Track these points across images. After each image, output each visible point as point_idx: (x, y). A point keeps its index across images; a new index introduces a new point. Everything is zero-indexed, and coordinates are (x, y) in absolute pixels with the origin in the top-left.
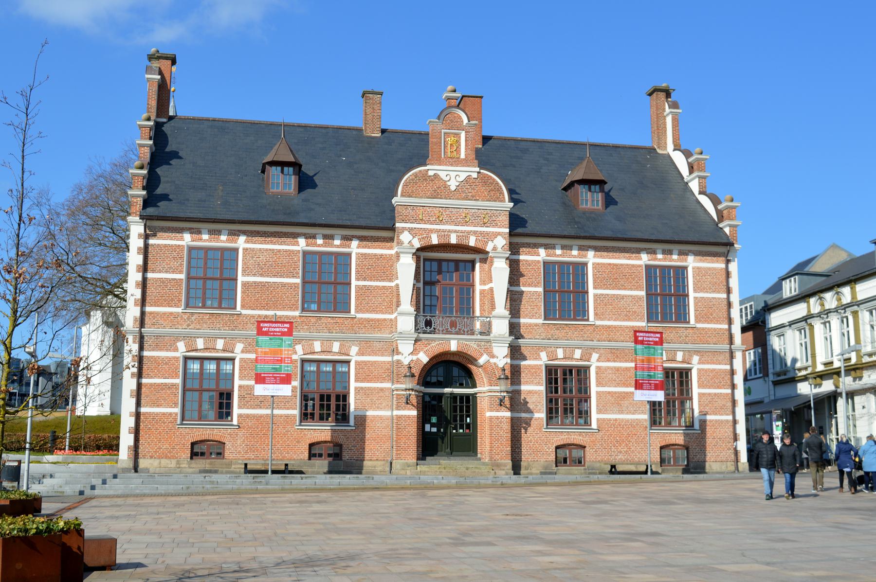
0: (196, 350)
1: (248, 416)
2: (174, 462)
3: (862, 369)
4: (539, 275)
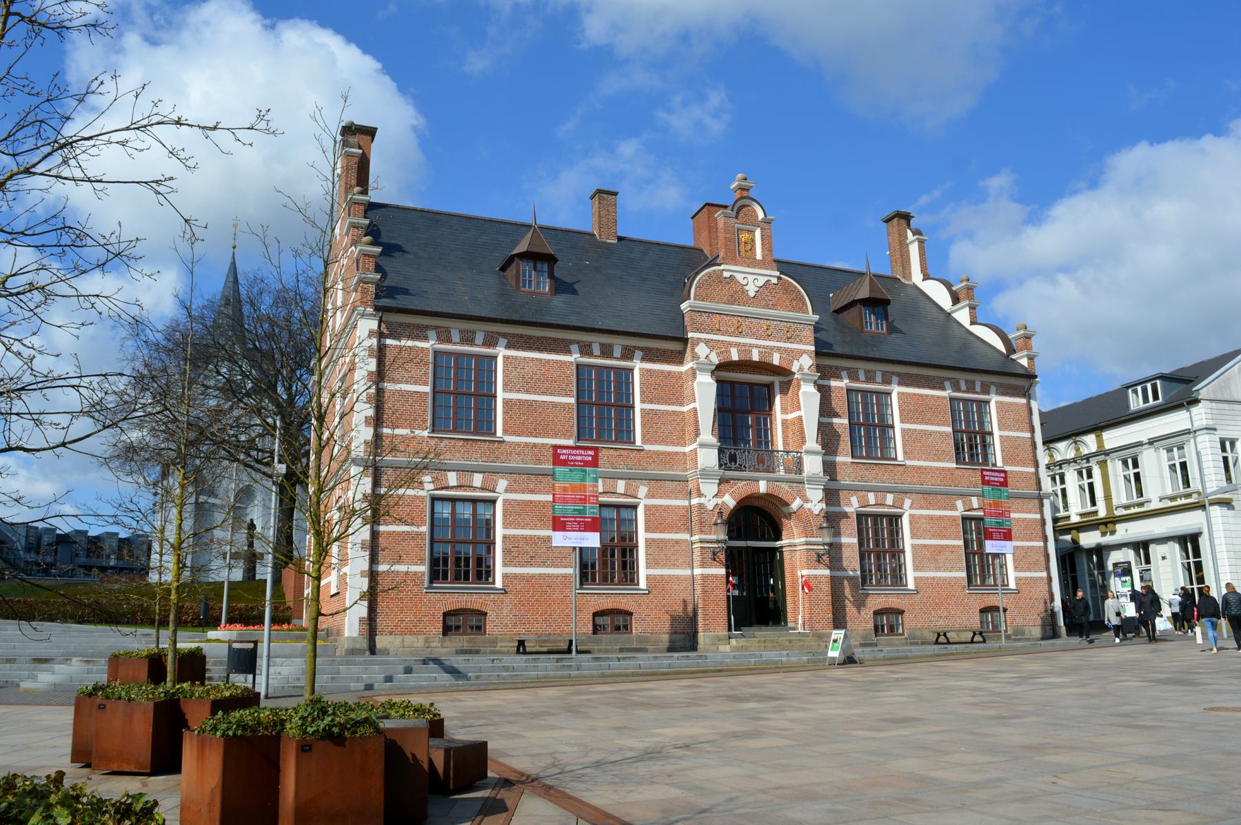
0: (447, 488)
1: (515, 576)
2: (421, 638)
3: (1114, 523)
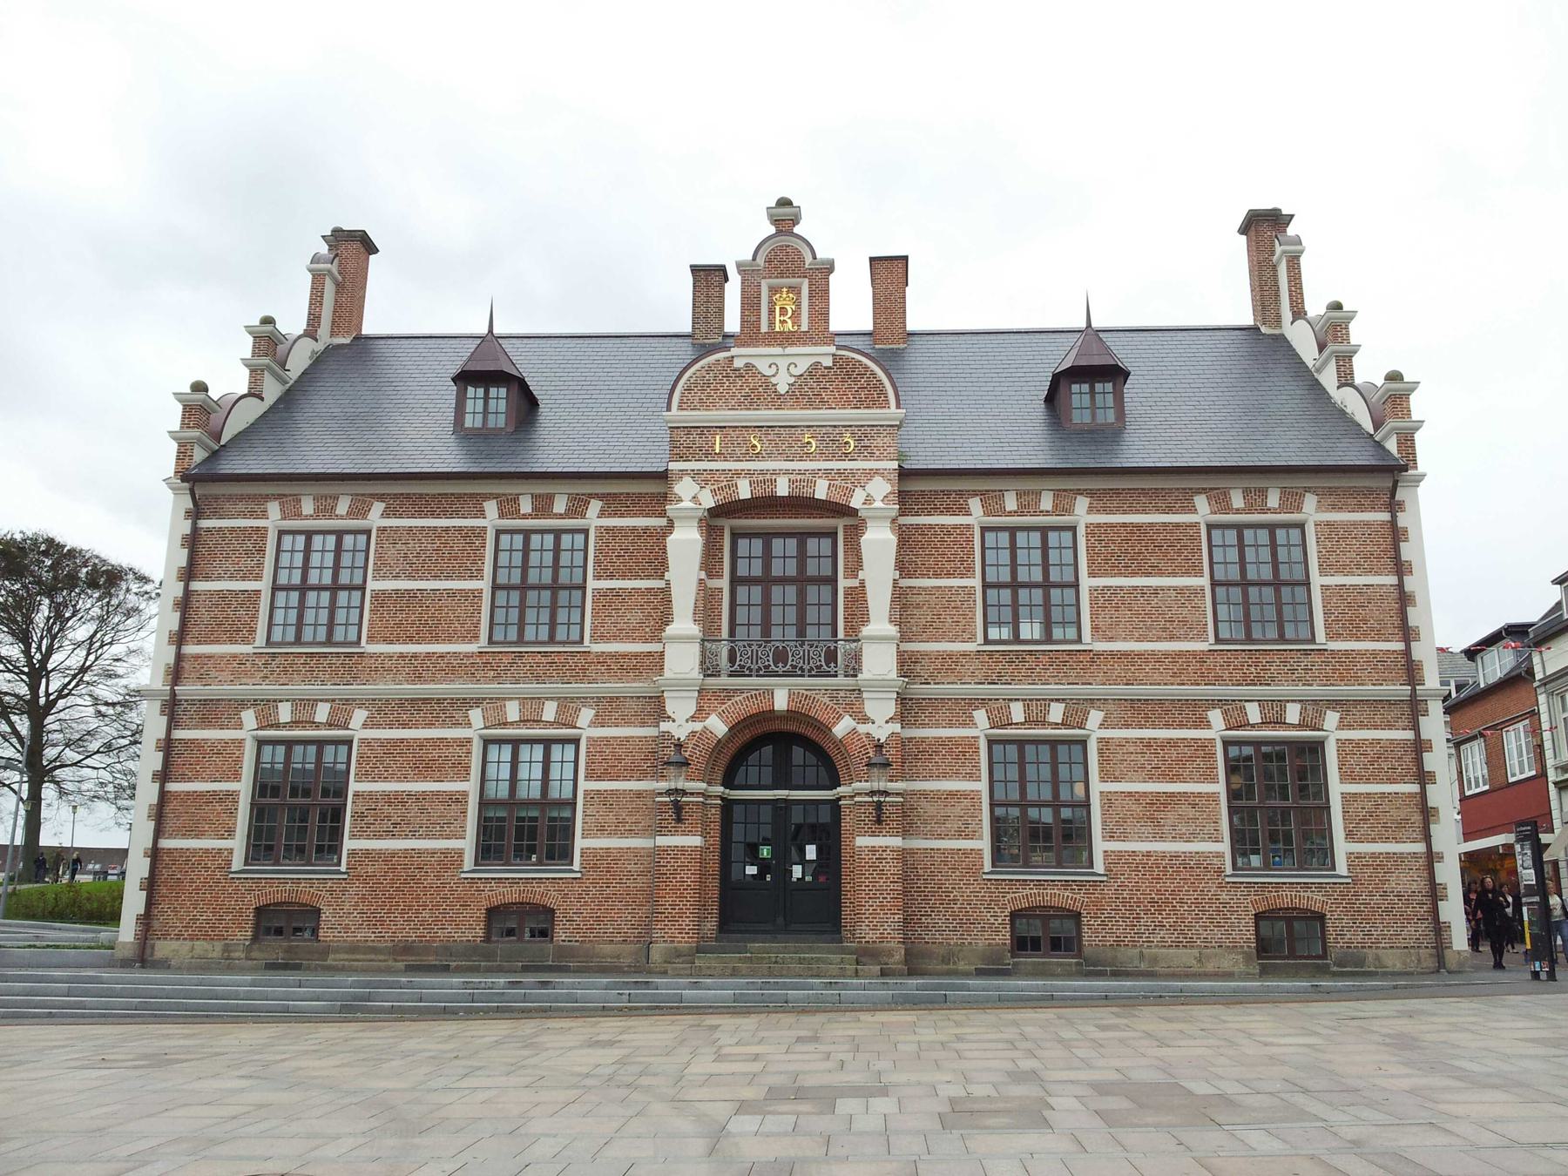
1: (367, 853)
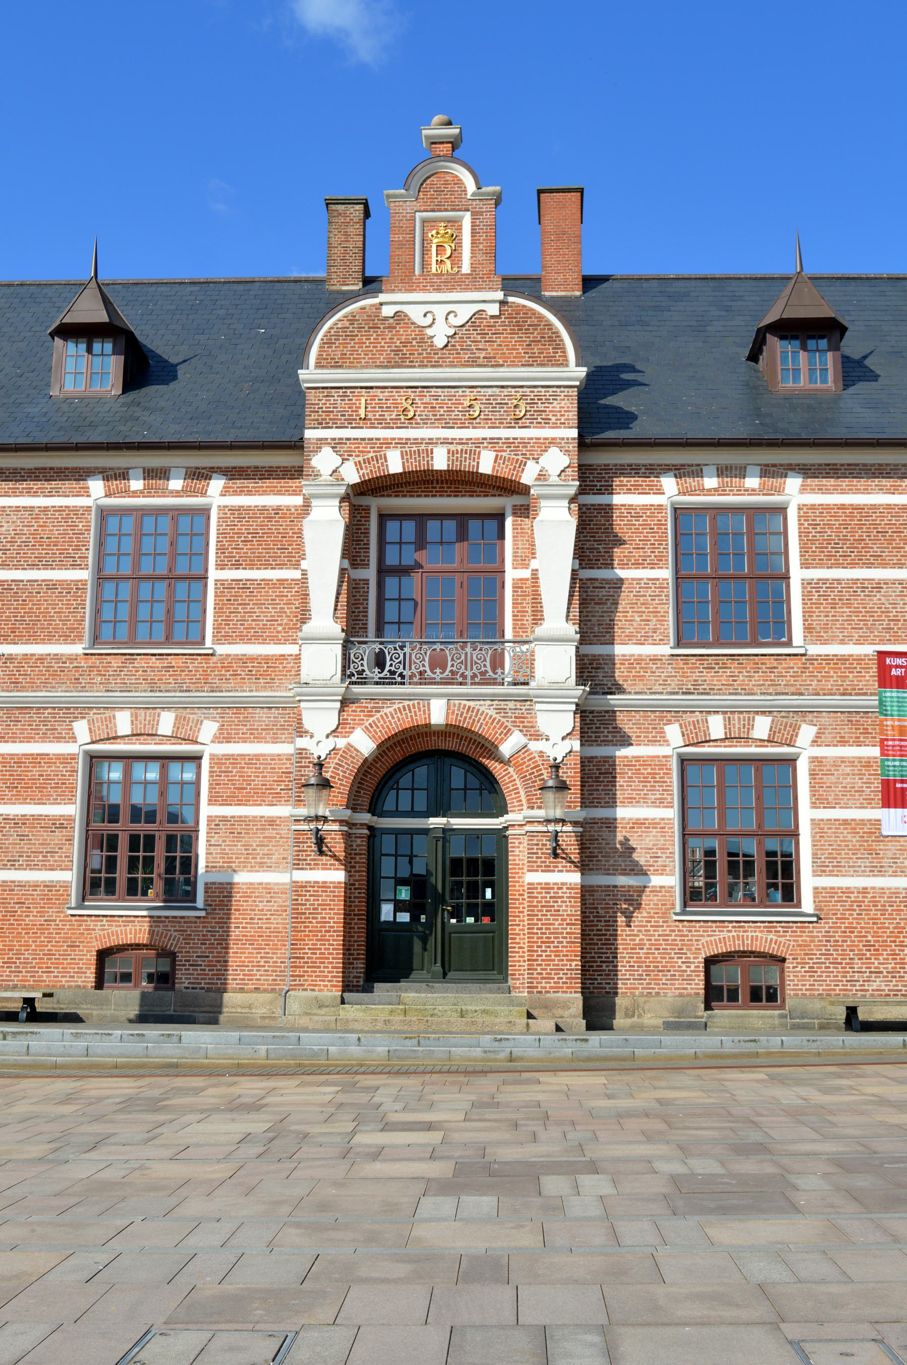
4: (662, 539)
